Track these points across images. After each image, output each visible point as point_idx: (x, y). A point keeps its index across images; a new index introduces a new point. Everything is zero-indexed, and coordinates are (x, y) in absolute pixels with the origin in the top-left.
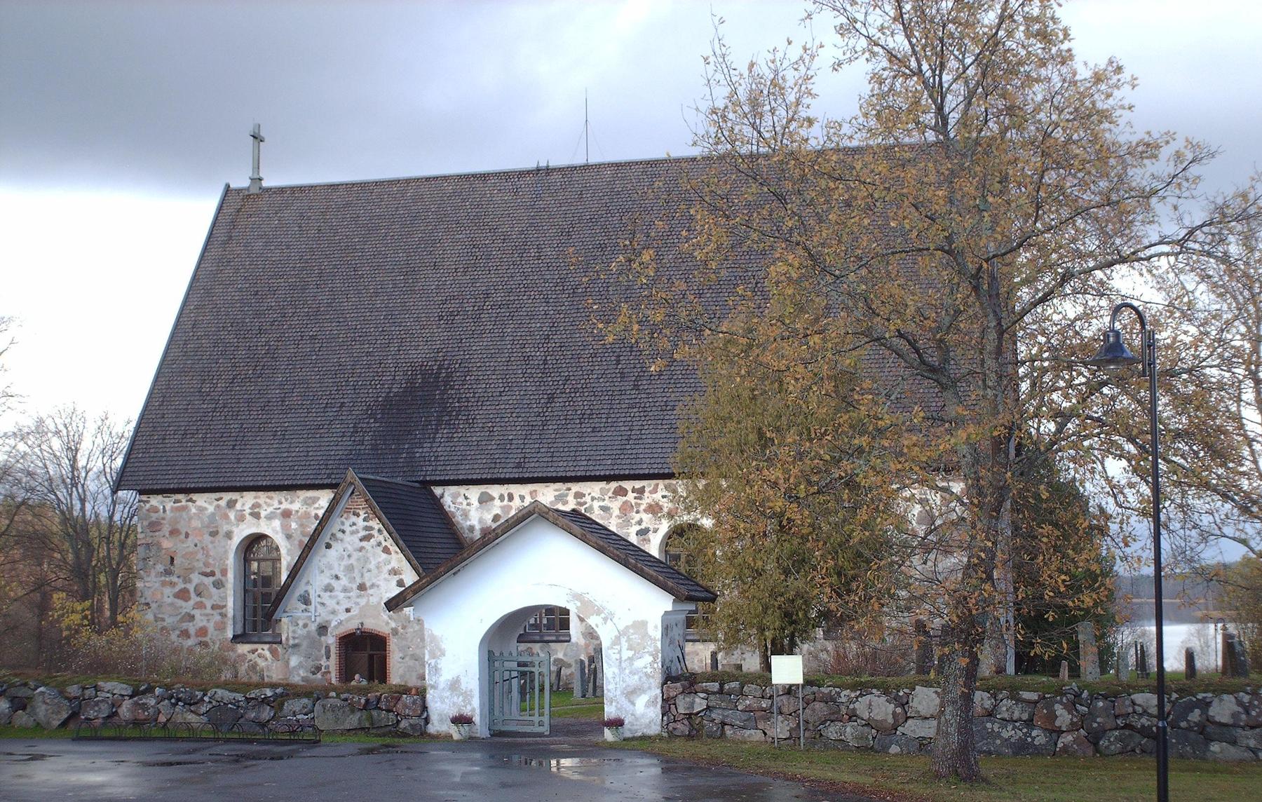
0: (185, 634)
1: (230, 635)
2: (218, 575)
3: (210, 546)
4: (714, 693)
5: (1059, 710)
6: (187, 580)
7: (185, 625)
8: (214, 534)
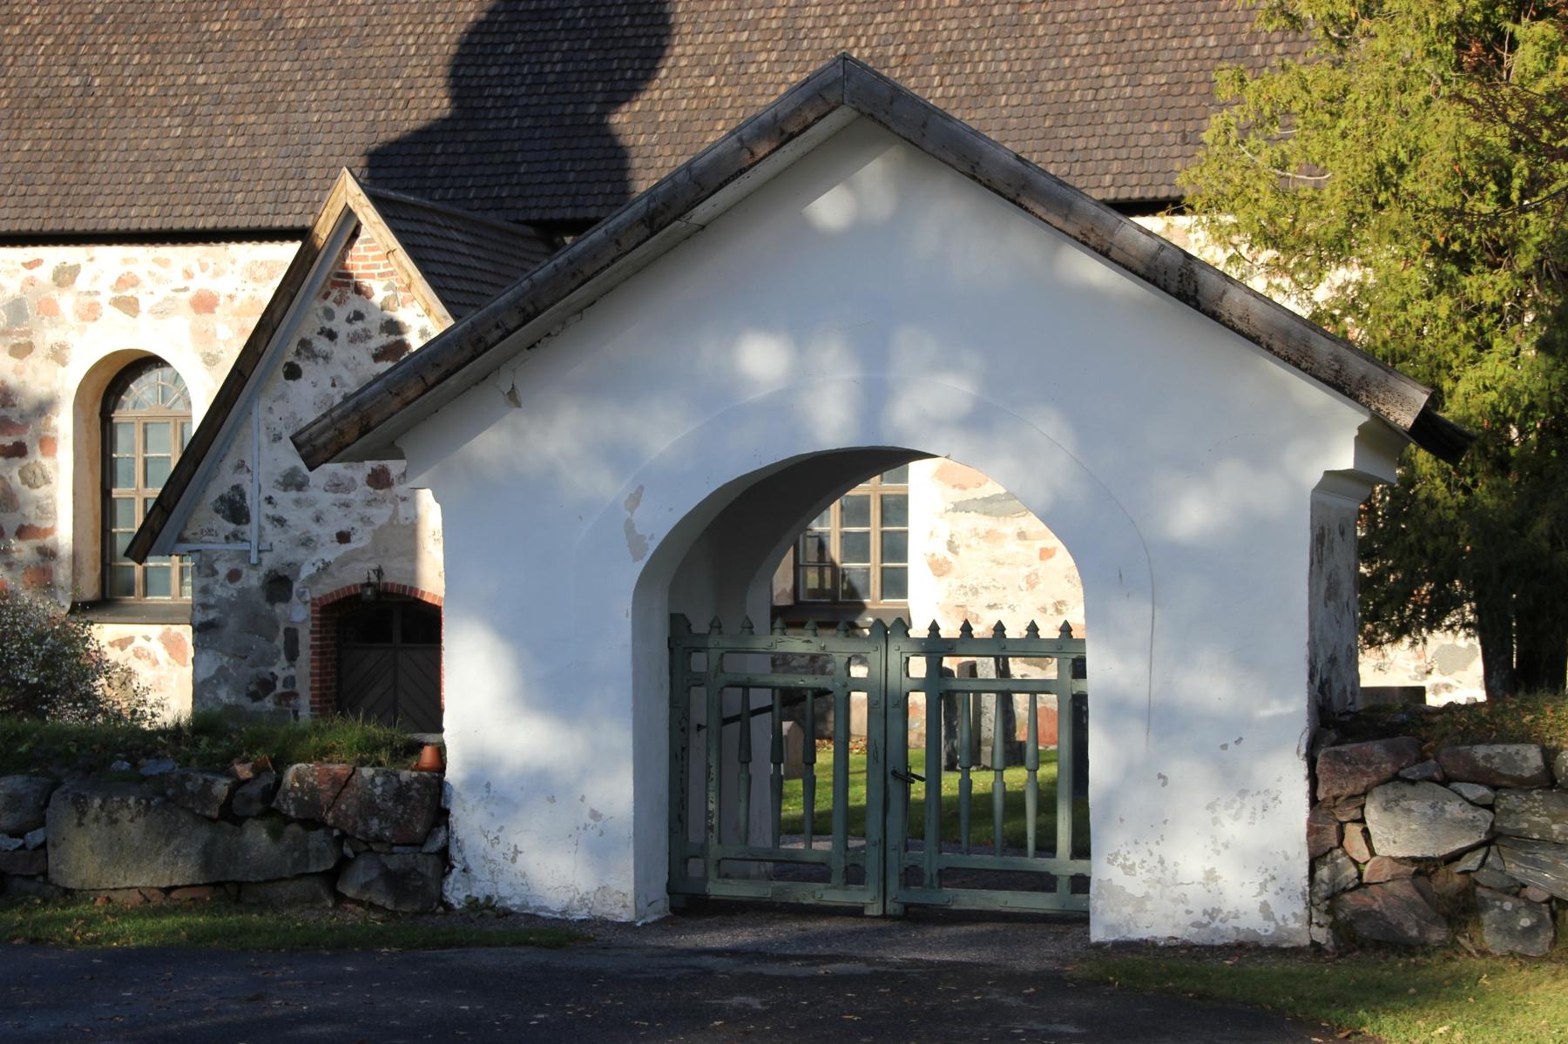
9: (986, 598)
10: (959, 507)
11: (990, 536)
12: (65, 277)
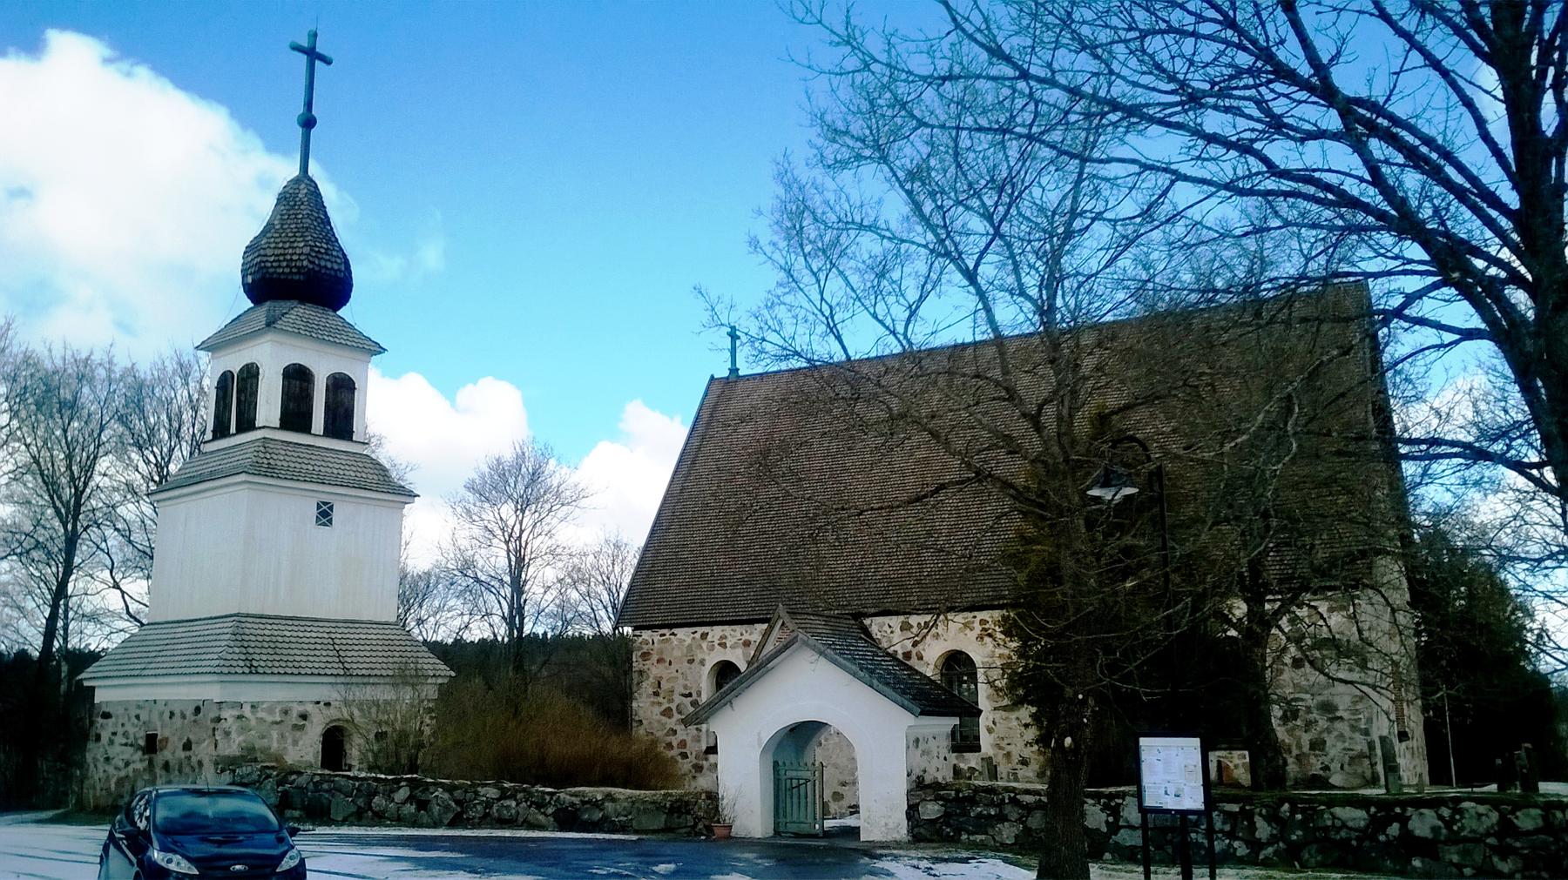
0: (670, 746)
1: (704, 748)
2: (695, 696)
3: (688, 672)
4: (950, 801)
5: (1260, 823)
6: (671, 701)
7: (668, 739)
8: (691, 661)
9: (1006, 742)
10: (995, 709)
11: (1006, 719)
12: (704, 636)
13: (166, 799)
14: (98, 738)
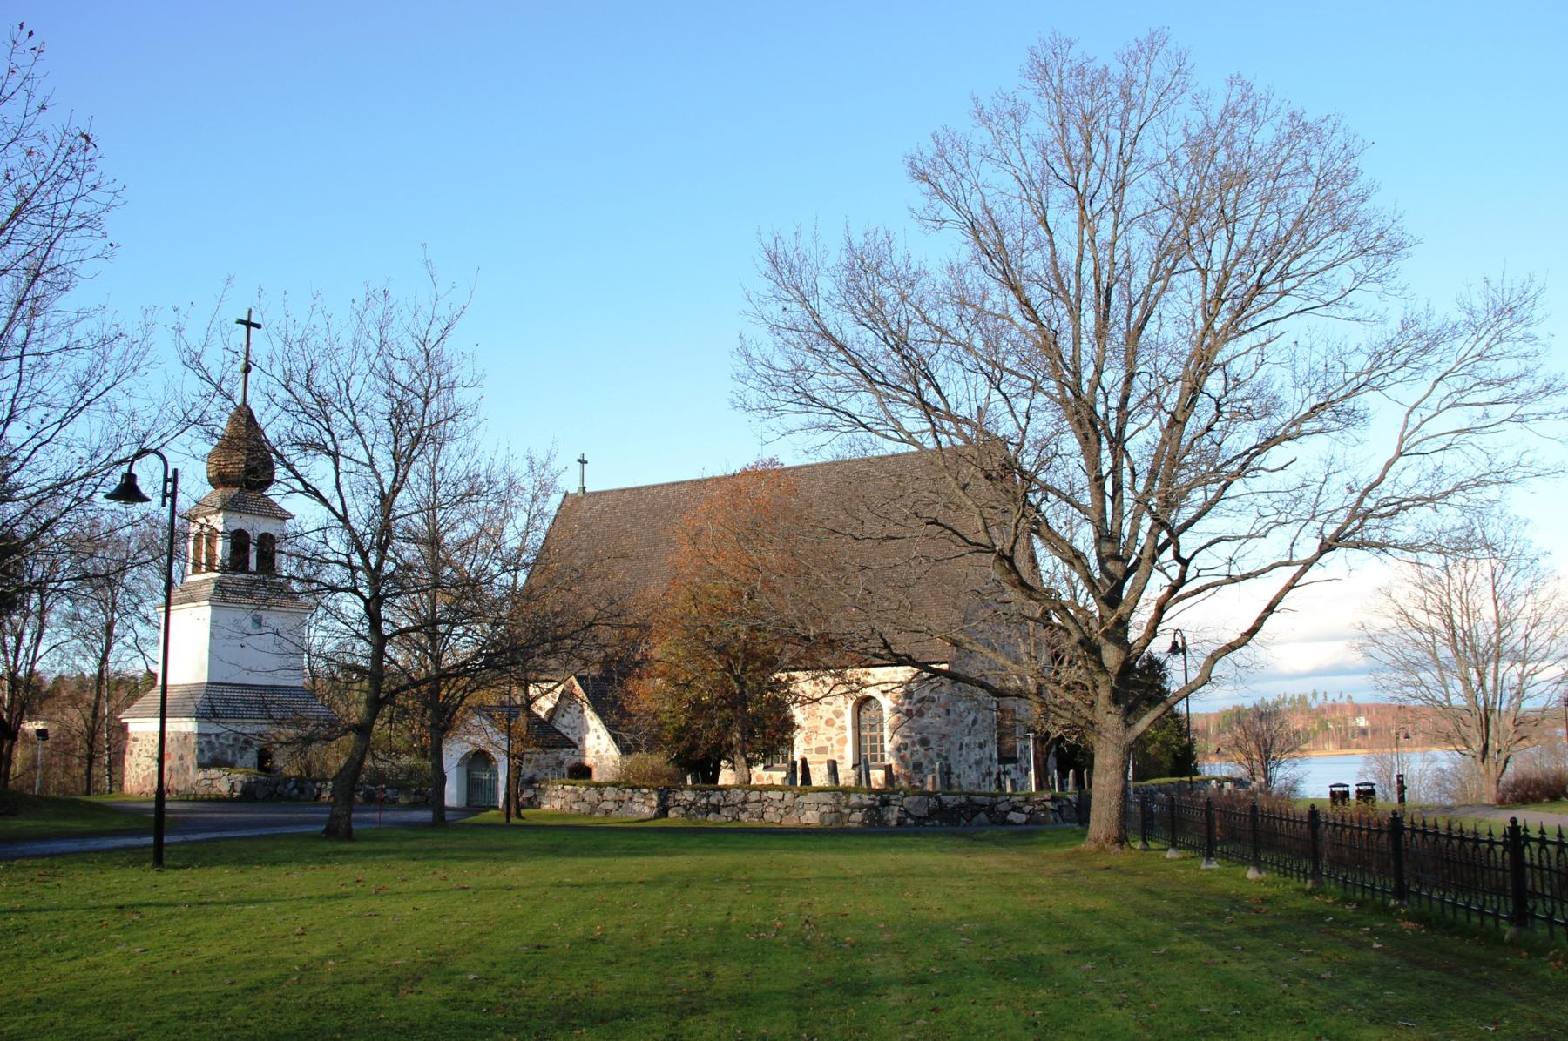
13: (242, 381)
14: (131, 753)
